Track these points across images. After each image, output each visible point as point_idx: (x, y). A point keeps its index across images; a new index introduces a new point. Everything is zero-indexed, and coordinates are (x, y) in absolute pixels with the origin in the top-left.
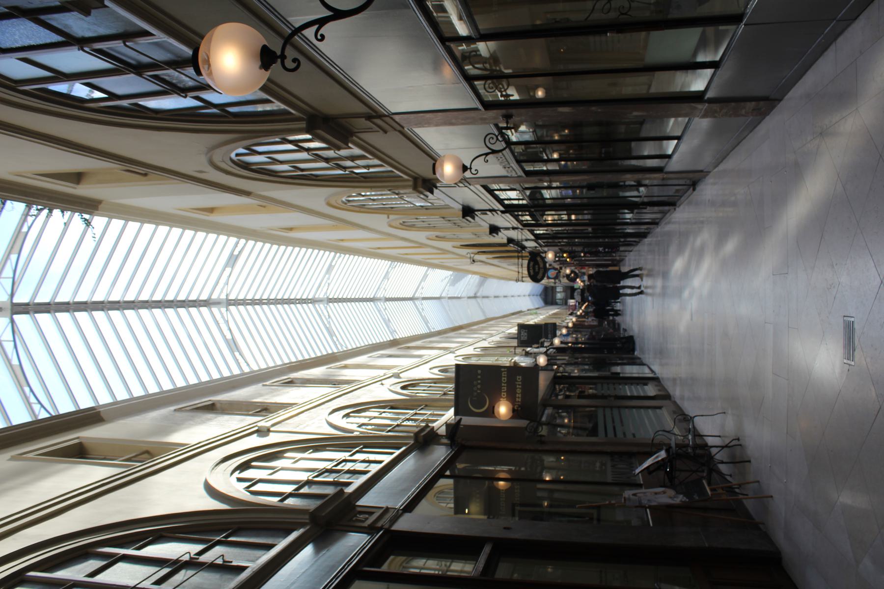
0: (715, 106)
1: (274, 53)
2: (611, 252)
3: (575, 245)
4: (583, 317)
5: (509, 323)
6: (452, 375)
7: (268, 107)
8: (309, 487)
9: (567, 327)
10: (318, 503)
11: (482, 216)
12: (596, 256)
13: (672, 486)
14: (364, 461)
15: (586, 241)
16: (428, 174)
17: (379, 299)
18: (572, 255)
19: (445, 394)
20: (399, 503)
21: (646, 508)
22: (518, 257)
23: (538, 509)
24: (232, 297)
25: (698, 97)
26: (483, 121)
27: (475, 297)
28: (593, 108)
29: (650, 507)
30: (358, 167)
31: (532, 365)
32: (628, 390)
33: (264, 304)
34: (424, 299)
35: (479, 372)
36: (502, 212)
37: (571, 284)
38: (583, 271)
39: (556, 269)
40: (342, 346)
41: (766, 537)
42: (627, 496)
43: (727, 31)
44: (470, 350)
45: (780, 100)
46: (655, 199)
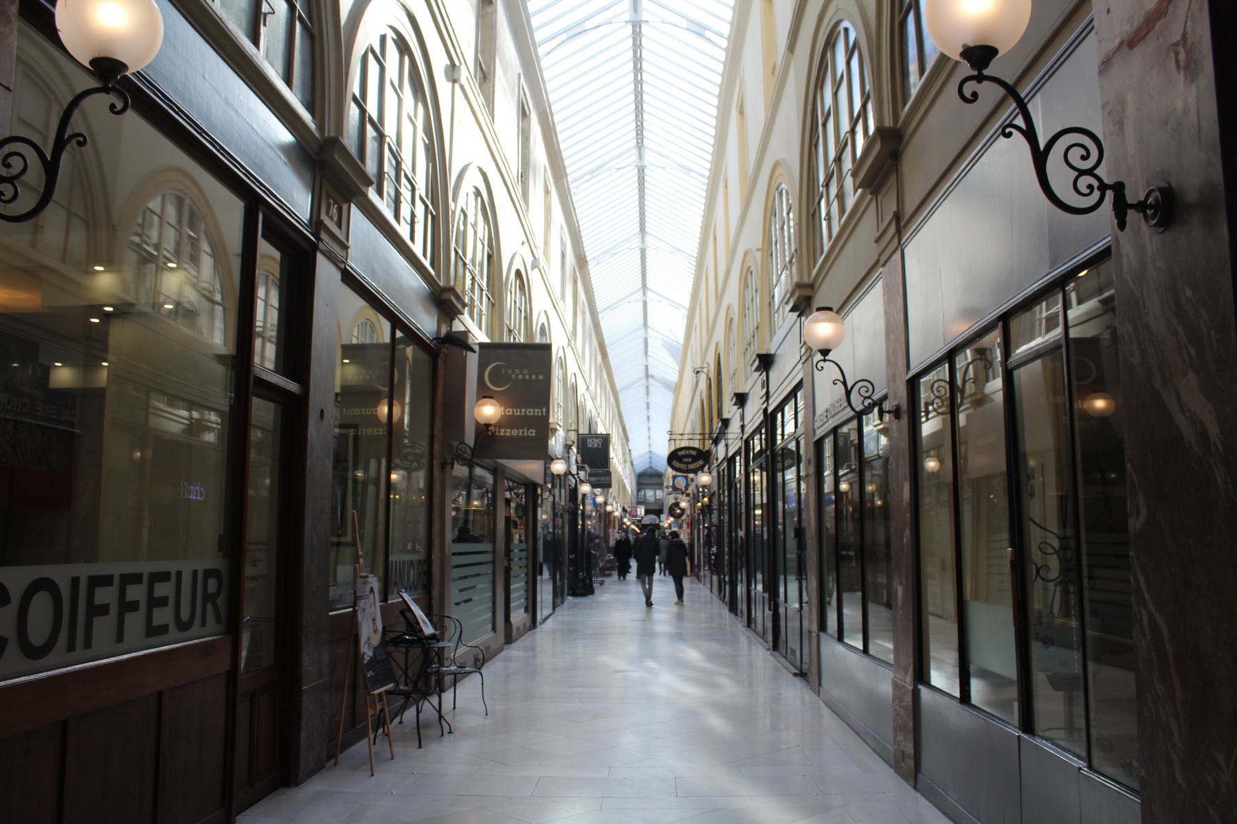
0: (908, 699)
1: (986, 65)
2: (710, 563)
3: (721, 513)
4: (621, 528)
5: (611, 424)
6: (538, 340)
7: (913, 67)
8: (374, 138)
9: (606, 503)
10: (353, 150)
11: (760, 382)
12: (705, 543)
13: (384, 642)
14: (413, 216)
15: (726, 529)
16: (817, 303)
18: (707, 510)
19: (510, 331)
20: (355, 264)
21: (354, 606)
22: (703, 434)
23: (351, 464)
24: (645, 29)
25: (921, 676)
26: (892, 378)
27: (647, 376)
28: (908, 532)
29: (355, 612)
30: (828, 204)
31: (550, 452)
32: (518, 586)
33: (636, 76)
34: (645, 303)
35: (541, 377)
36: (765, 410)
37: (666, 510)
38: (685, 526)
39: (687, 487)
40: (577, 187)
41: (318, 768)
42: (369, 579)
43: (1012, 713)
44: (572, 367)
45: (915, 788)
46: (782, 624)
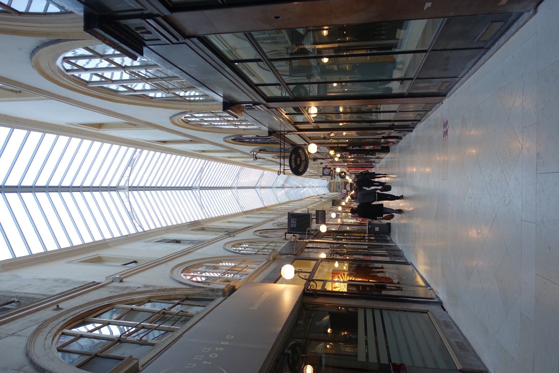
17: (196, 188)
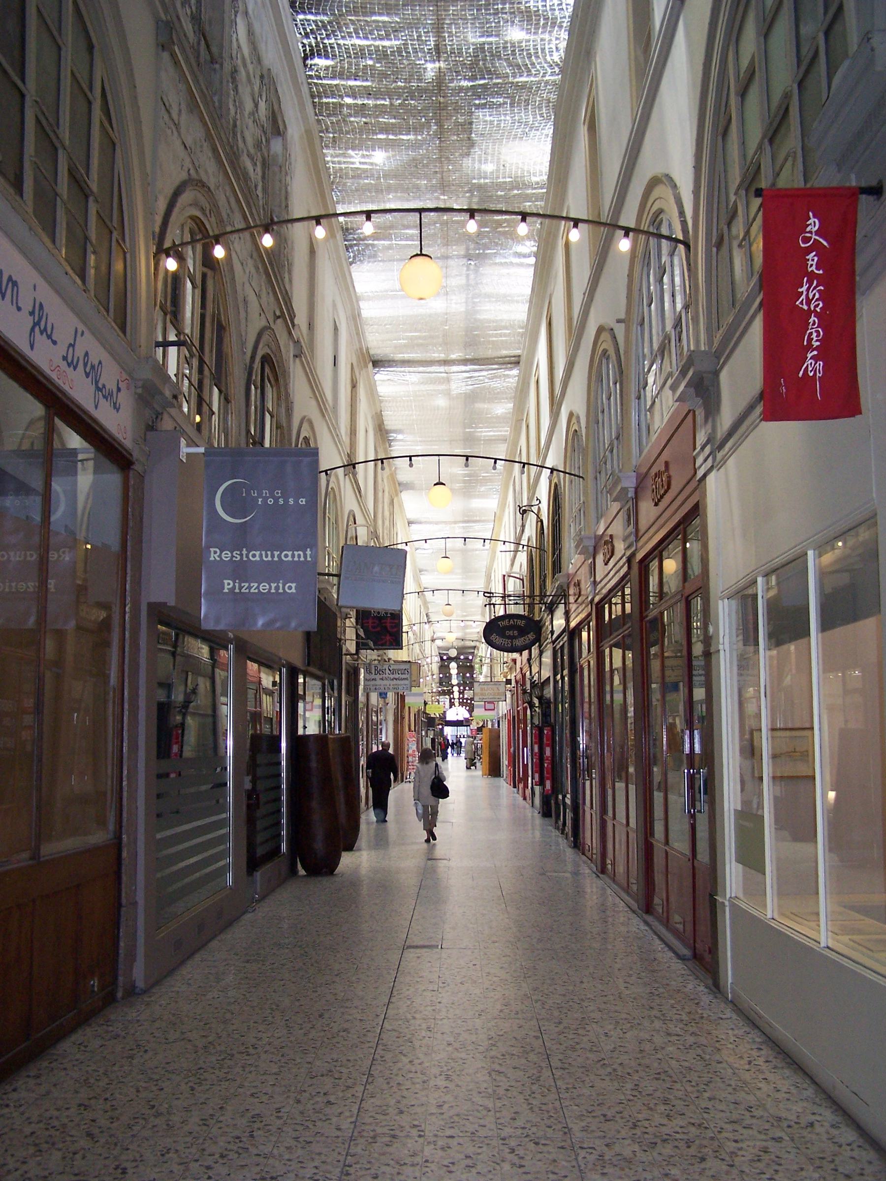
22: (532, 596)
35: (303, 501)
